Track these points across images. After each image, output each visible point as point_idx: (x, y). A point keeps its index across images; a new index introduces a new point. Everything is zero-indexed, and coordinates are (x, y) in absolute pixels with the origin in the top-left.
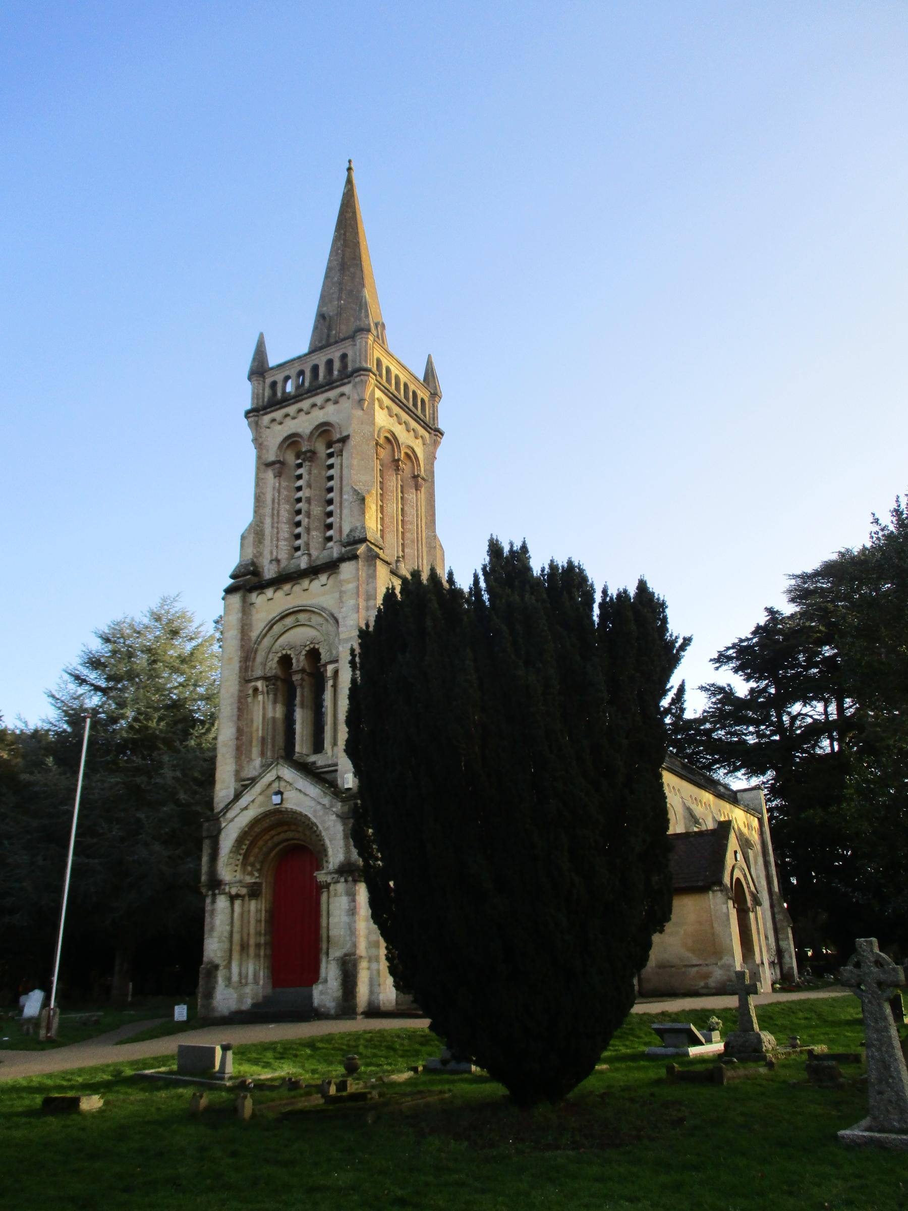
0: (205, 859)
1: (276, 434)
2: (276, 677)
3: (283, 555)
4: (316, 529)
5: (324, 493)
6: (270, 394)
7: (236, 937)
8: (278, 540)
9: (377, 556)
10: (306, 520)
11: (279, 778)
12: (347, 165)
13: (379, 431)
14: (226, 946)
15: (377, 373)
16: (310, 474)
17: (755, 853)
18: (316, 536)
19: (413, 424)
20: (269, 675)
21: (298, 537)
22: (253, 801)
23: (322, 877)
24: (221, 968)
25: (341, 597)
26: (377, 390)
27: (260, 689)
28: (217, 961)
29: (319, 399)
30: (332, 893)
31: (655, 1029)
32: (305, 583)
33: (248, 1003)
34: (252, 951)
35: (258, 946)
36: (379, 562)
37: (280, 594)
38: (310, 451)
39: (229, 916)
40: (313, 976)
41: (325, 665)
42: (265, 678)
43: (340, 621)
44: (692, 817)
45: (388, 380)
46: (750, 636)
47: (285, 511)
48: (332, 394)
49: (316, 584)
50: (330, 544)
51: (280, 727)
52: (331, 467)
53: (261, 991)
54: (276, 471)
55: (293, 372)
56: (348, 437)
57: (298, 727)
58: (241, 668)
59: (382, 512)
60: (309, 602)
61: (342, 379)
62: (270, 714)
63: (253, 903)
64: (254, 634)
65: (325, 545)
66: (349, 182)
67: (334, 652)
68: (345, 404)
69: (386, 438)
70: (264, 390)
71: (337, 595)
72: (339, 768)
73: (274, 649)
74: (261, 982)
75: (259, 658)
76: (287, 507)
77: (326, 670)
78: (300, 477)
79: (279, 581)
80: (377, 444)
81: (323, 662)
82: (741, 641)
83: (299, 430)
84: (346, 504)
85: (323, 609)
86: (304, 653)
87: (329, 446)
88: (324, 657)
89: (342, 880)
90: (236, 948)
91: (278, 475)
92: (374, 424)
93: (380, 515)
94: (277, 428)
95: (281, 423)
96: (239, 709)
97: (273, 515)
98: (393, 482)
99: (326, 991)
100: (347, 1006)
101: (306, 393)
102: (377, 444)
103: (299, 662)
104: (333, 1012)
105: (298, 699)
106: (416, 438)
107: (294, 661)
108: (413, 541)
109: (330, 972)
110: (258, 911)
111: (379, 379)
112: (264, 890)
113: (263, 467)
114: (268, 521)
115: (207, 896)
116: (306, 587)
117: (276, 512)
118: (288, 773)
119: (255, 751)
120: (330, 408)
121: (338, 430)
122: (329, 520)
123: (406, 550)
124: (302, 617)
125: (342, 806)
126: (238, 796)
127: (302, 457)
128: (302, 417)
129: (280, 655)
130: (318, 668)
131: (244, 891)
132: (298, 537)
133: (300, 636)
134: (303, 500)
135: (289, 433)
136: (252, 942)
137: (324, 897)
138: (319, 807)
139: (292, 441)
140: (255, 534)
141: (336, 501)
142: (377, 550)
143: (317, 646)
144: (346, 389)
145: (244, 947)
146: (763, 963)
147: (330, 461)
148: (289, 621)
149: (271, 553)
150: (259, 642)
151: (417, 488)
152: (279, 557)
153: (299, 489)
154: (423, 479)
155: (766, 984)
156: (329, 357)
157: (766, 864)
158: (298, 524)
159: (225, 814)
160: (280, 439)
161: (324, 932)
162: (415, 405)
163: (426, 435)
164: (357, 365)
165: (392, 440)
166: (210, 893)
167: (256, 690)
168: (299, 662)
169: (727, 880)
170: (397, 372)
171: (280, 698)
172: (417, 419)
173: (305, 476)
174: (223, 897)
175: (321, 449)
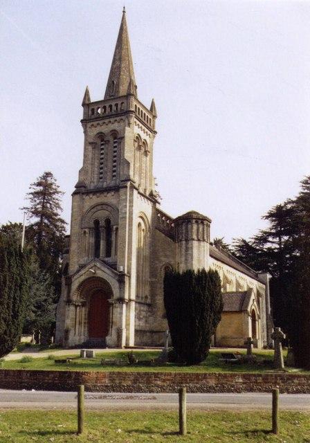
1: (94, 132)
2: (93, 228)
6: (92, 114)
11: (95, 266)
17: (262, 300)
31: (235, 358)
32: (105, 194)
34: (83, 324)
35: (85, 323)
41: (113, 226)
42: (90, 228)
44: (238, 285)
48: (118, 119)
49: (109, 195)
60: (106, 201)
88: (112, 223)
90: (77, 323)
91: (94, 148)
98: (138, 154)
99: (110, 339)
100: (127, 347)
103: (102, 223)
109: (113, 332)
120: (116, 124)
124: (104, 206)
126: (78, 271)
133: (102, 214)
140: (82, 172)
144: (123, 117)
145: (80, 323)
146: (129, 272)
148: (99, 207)
151: (146, 155)
155: (261, 344)
157: (267, 304)
167: (85, 232)
168: (102, 223)
169: (249, 310)
172: (148, 128)
175: (111, 139)
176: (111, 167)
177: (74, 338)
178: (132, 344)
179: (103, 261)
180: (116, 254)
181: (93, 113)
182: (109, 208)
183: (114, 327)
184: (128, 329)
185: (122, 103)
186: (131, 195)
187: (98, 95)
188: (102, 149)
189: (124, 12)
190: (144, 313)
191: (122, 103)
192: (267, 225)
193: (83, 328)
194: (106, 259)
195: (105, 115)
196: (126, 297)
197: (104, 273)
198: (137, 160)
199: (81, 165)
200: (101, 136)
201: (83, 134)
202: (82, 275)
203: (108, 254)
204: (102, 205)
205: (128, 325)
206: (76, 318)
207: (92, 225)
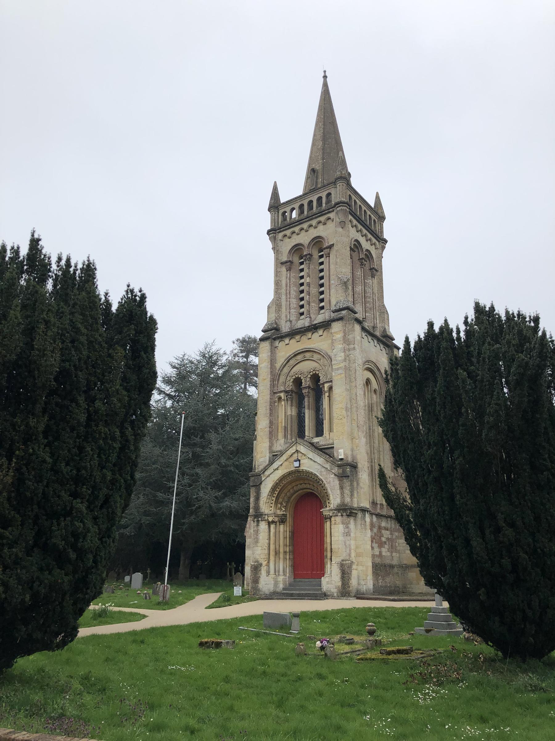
1: (287, 245)
2: (292, 391)
12: (323, 74)
14: (266, 552)
22: (281, 465)
32: (309, 335)
34: (281, 556)
35: (285, 552)
42: (286, 392)
48: (322, 219)
49: (316, 335)
56: (333, 245)
66: (325, 85)
68: (330, 224)
90: (272, 553)
91: (289, 269)
95: (290, 238)
103: (306, 382)
114: (284, 297)
120: (321, 227)
124: (308, 355)
126: (271, 463)
133: (305, 367)
140: (275, 305)
145: (277, 553)
148: (299, 357)
167: (280, 398)
168: (306, 382)
176: (317, 257)
177: (266, 583)
180: (331, 430)
181: (284, 218)
182: (316, 357)
183: (336, 560)
187: (293, 188)
188: (302, 270)
189: (325, 77)
190: (386, 534)
191: (329, 195)
194: (316, 440)
195: (302, 217)
197: (312, 463)
199: (270, 296)
200: (297, 249)
201: (272, 252)
202: (277, 469)
203: (319, 432)
204: (295, 355)
206: (269, 544)
207: (290, 385)
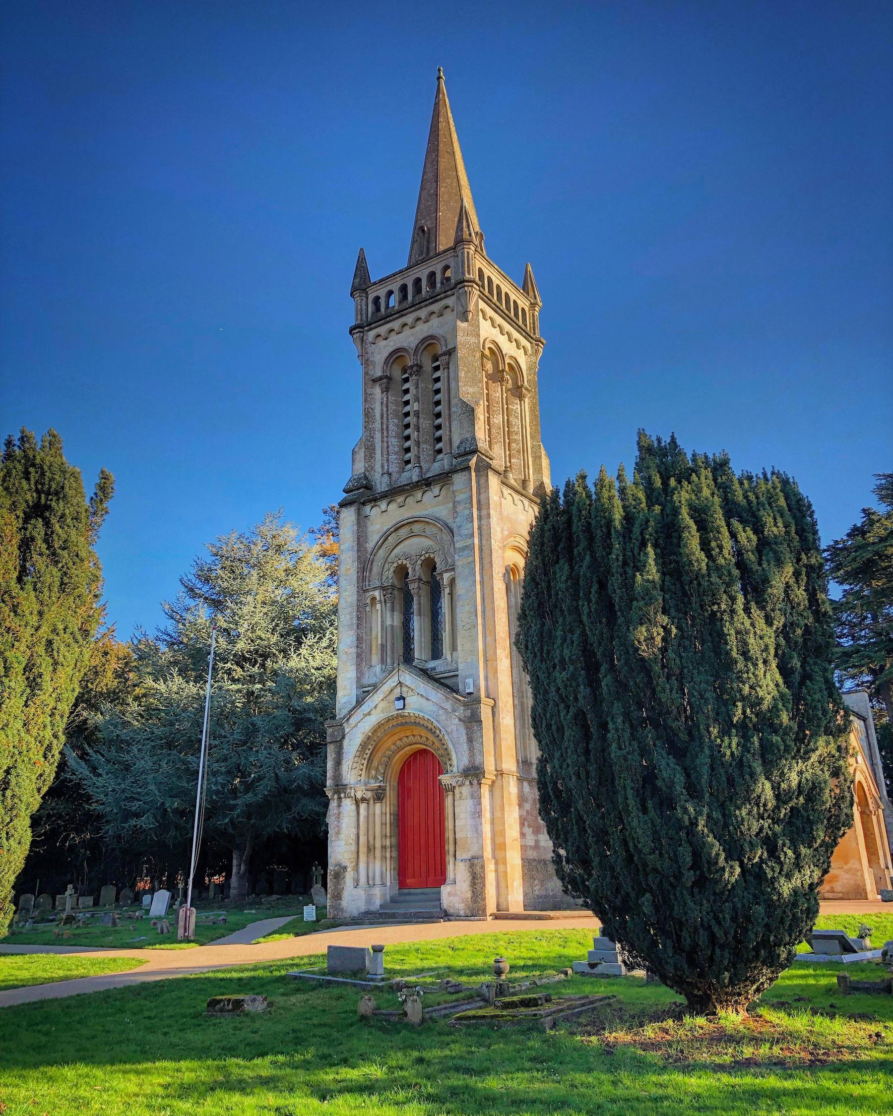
0: (330, 764)
1: (381, 351)
2: (393, 586)
3: (394, 469)
4: (425, 442)
5: (432, 393)
7: (363, 839)
8: (388, 454)
9: (489, 467)
10: (416, 433)
13: (484, 342)
14: (353, 848)
15: (480, 283)
16: (417, 388)
18: (427, 449)
19: (516, 335)
20: (386, 584)
21: (408, 450)
23: (445, 779)
24: (349, 869)
25: (454, 507)
26: (480, 301)
27: (378, 599)
28: (345, 863)
29: (423, 313)
30: (457, 796)
33: (377, 902)
34: (378, 853)
35: (384, 847)
36: (491, 474)
37: (393, 506)
38: (417, 365)
39: (354, 819)
40: (440, 877)
41: (441, 574)
42: (383, 588)
43: (455, 530)
45: (491, 291)
46: (845, 538)
47: (393, 425)
48: (435, 307)
49: (429, 495)
50: (440, 456)
51: (399, 634)
52: (437, 380)
53: (388, 892)
54: (384, 386)
55: (395, 286)
57: (416, 634)
58: (358, 578)
59: (489, 425)
61: (446, 292)
62: (389, 622)
63: (378, 806)
64: (370, 545)
65: (435, 457)
67: (450, 560)
68: (449, 316)
69: (490, 348)
70: (367, 305)
71: (451, 505)
72: (459, 673)
73: (390, 560)
74: (388, 884)
75: (376, 569)
76: (396, 421)
77: (442, 579)
78: (407, 391)
79: (391, 494)
80: (483, 355)
81: (438, 571)
82: (836, 542)
83: (405, 345)
84: (454, 416)
85: (437, 519)
86: (419, 562)
87: (435, 359)
89: (467, 783)
90: (363, 849)
91: (386, 390)
92: (479, 336)
93: (487, 427)
94: (382, 343)
95: (386, 339)
96: (358, 618)
97: (382, 429)
98: (497, 392)
99: (454, 893)
101: (410, 307)
102: (483, 355)
104: (462, 913)
105: (415, 606)
106: (518, 348)
107: (410, 571)
108: (519, 451)
109: (458, 871)
110: (383, 814)
111: (482, 289)
112: (388, 794)
113: (370, 382)
114: (378, 436)
115: (333, 799)
116: (419, 499)
117: (385, 427)
118: (409, 678)
119: (375, 658)
120: (435, 321)
121: (443, 343)
122: (438, 434)
123: (513, 460)
124: (416, 528)
125: (464, 710)
126: (359, 702)
127: (409, 372)
128: (407, 331)
129: (395, 565)
130: (434, 577)
131: (369, 795)
132: (408, 450)
133: (415, 546)
134: (412, 414)
135: (394, 348)
136: (378, 844)
137: (449, 801)
138: (441, 712)
139: (396, 355)
141: (445, 414)
142: (488, 460)
143: (432, 556)
144: (450, 301)
145: (370, 849)
147: (436, 375)
148: (403, 532)
149: (383, 467)
150: (374, 552)
152: (390, 471)
153: (407, 403)
154: (527, 389)
156: (431, 269)
158: (408, 438)
159: (348, 720)
160: (386, 355)
161: (449, 835)
162: (516, 315)
163: (528, 345)
164: (460, 277)
165: (496, 353)
166: (336, 796)
167: (374, 599)
168: (415, 571)
170: (499, 283)
171: (397, 606)
172: (519, 329)
173: (413, 390)
174: (348, 800)
178: (516, 900)
179: (421, 670)
180: (454, 648)
184: (500, 860)
185: (447, 267)
186: (483, 488)
192: (325, 951)
193: (378, 864)
194: (432, 664)
196: (489, 766)
198: (497, 407)
203: (436, 654)
205: (499, 847)
